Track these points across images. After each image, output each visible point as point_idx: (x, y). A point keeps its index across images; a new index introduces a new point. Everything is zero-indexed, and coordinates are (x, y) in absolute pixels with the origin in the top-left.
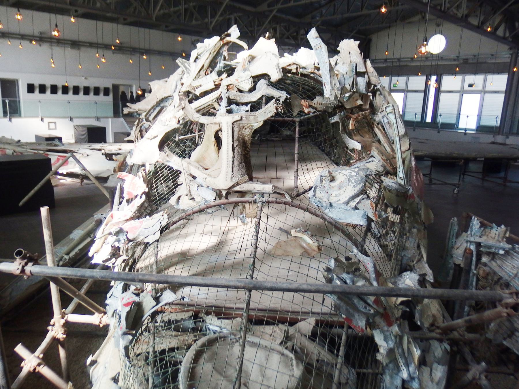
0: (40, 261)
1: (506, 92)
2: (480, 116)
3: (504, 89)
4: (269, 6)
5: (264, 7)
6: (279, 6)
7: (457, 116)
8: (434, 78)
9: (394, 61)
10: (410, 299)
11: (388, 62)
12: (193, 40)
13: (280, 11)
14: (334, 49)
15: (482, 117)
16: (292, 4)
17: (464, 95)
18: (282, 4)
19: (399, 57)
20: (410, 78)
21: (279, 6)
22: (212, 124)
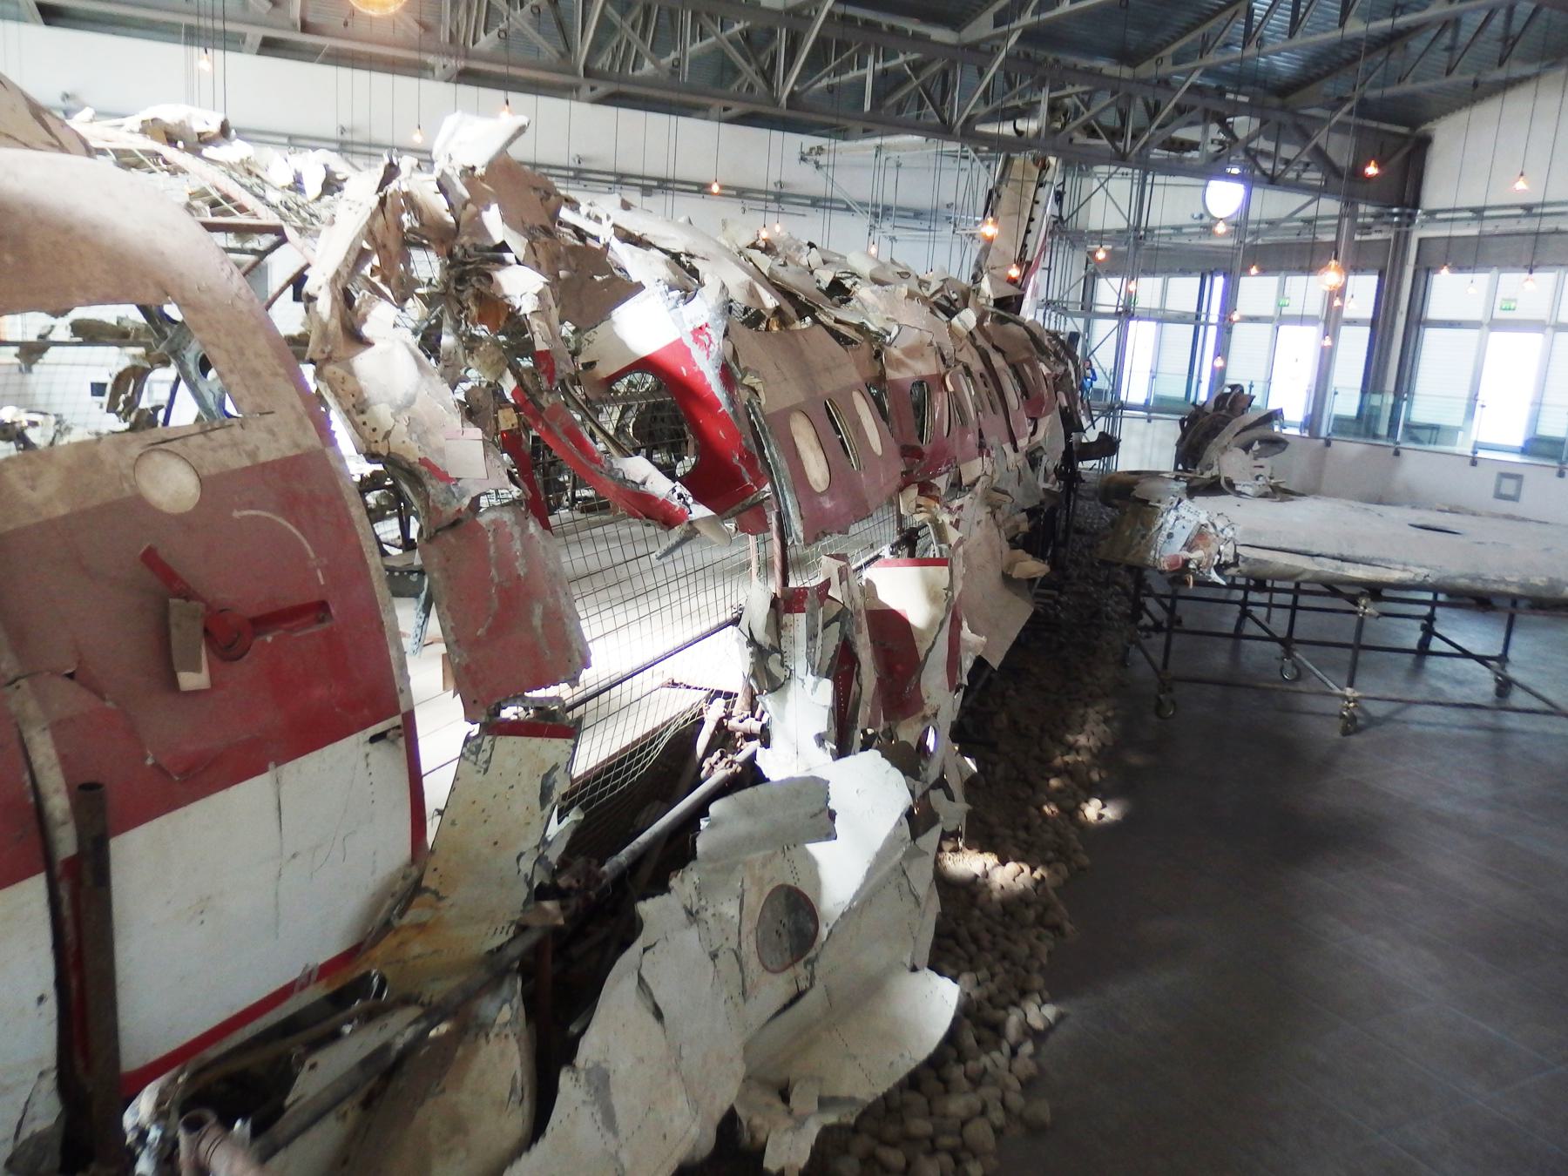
0: (474, 43)
1: (1373, 323)
2: (1538, 406)
3: (1369, 315)
4: (999, 20)
5: (982, 28)
6: (1028, 19)
7: (1468, 405)
8: (1219, 281)
9: (1163, 235)
10: (725, 406)
11: (1185, 234)
12: (806, 150)
13: (1028, 36)
14: (1269, 172)
15: (1543, 408)
16: (1066, 7)
17: (1281, 328)
18: (1035, 12)
19: (1478, 202)
20: (1288, 278)
21: (1028, 19)
22: (981, 436)
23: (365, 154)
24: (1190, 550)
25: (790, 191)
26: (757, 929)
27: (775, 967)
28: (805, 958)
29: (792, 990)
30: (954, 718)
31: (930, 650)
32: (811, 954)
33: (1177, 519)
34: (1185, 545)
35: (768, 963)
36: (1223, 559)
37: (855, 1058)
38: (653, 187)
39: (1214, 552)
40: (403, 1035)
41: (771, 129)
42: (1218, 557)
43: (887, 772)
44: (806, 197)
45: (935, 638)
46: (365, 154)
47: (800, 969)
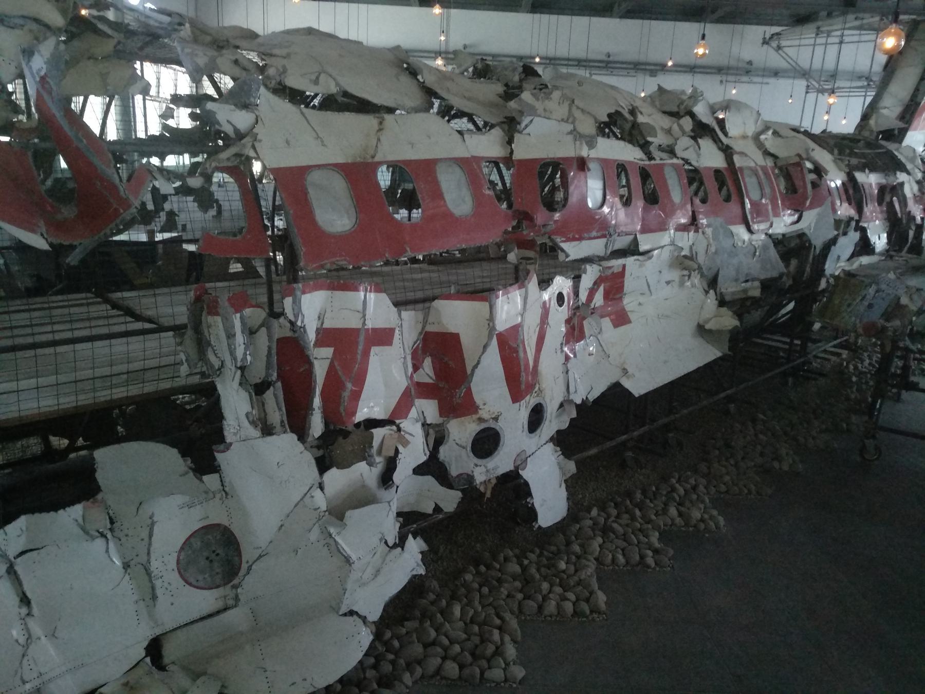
23: (566, 65)
24: (887, 320)
25: (616, 59)
26: (180, 552)
27: (201, 584)
28: (232, 584)
29: (220, 605)
30: (225, 422)
31: (476, 366)
32: (236, 581)
33: (877, 291)
34: (882, 315)
35: (192, 580)
36: (915, 328)
37: (265, 671)
38: (657, 70)
39: (907, 322)
40: (632, 533)
41: (558, 14)
42: (910, 327)
43: (301, 453)
44: (630, 63)
45: (480, 358)
46: (566, 65)
47: (226, 590)
